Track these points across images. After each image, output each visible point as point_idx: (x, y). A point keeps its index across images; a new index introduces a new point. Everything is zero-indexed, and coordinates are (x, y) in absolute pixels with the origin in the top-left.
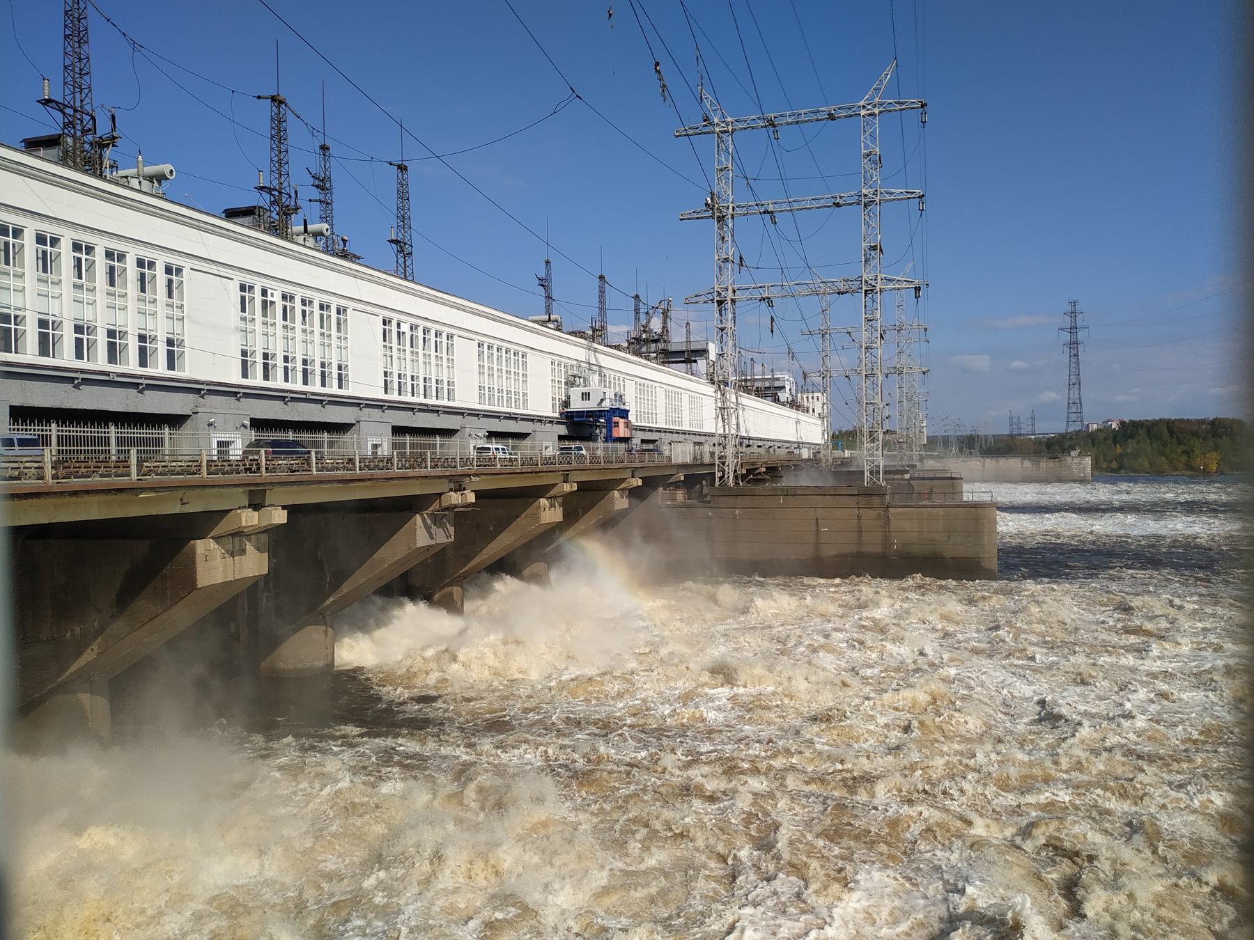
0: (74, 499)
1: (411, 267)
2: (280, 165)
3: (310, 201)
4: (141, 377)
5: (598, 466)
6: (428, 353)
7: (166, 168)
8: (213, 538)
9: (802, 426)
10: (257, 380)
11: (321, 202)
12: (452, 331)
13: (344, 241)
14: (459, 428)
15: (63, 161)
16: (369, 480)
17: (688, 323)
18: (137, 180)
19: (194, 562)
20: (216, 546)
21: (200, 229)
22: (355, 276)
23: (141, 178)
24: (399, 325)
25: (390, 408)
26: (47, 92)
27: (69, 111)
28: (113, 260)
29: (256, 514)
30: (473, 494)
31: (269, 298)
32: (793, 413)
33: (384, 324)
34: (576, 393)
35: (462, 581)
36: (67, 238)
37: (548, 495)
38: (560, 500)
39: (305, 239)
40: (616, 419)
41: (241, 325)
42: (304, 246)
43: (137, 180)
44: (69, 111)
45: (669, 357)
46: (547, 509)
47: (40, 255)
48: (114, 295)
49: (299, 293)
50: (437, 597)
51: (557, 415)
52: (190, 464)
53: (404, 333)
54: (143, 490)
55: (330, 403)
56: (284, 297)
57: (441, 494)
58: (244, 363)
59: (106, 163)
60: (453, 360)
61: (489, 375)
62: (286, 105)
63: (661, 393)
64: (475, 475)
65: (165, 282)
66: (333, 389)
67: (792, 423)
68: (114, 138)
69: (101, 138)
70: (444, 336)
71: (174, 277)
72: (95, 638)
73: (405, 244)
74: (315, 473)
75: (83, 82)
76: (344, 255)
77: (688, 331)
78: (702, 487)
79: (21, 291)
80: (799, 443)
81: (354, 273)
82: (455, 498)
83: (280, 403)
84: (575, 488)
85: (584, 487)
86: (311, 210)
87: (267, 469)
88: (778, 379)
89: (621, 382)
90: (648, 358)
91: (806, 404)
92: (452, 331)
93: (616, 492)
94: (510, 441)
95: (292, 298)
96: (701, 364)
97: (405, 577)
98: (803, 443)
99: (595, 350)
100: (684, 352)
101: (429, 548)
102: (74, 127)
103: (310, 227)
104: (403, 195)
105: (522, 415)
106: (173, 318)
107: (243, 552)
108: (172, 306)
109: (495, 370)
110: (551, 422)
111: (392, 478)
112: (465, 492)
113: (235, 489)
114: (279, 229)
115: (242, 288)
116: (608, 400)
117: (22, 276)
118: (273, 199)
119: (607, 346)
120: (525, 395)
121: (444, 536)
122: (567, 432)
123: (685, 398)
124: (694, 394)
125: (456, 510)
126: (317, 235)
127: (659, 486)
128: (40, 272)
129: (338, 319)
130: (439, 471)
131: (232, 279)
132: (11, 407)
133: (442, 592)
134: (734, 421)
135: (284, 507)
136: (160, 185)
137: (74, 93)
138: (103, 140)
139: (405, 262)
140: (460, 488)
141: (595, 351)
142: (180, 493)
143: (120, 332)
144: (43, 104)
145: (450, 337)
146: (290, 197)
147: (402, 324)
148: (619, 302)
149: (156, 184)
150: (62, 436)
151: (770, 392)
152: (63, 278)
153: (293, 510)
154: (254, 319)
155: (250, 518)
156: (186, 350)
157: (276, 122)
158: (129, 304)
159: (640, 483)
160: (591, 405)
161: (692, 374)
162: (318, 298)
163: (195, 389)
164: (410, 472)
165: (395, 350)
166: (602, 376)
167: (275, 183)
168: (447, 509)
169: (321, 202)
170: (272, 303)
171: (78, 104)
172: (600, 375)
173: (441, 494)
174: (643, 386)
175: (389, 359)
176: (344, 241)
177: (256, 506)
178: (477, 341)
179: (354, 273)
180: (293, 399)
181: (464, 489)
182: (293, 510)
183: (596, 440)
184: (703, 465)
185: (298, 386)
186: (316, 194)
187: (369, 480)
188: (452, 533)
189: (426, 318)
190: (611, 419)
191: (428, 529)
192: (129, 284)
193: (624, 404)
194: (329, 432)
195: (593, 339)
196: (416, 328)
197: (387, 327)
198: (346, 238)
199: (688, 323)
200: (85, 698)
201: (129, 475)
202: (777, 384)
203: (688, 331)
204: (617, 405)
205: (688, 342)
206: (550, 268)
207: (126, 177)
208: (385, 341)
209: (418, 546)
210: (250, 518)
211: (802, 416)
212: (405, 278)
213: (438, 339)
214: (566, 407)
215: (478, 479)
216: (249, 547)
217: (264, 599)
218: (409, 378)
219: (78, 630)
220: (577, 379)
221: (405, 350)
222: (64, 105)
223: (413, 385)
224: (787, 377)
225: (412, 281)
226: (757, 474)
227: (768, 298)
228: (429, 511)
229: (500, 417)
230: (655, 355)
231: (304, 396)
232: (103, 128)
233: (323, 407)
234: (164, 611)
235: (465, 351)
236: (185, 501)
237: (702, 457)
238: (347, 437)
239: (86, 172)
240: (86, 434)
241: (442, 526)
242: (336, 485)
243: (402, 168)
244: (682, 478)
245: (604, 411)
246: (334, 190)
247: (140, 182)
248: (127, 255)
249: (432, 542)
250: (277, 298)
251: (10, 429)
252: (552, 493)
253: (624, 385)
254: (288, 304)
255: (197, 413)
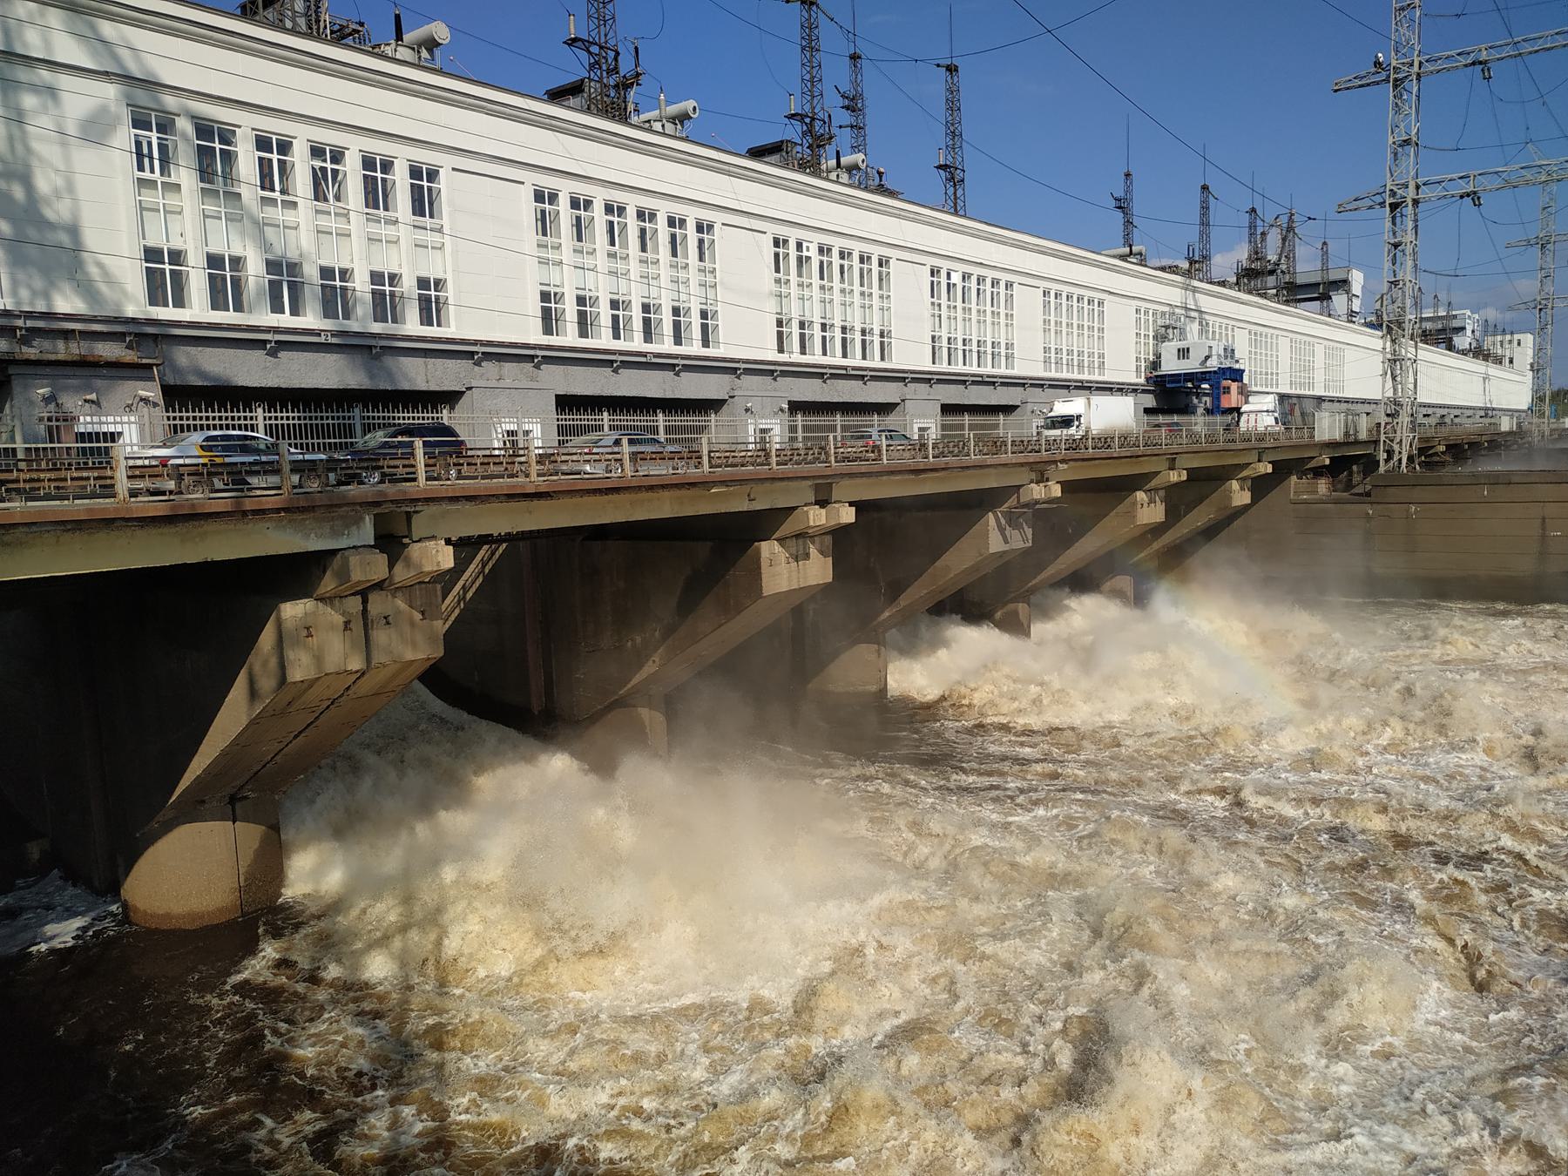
0: (650, 494)
1: (962, 198)
2: (812, 83)
3: (840, 127)
4: (676, 357)
5: (1215, 447)
6: (982, 308)
7: (689, 105)
8: (777, 540)
9: (1493, 385)
10: (569, 337)
11: (852, 127)
12: (887, 252)
13: (880, 174)
14: (1019, 404)
15: (785, 166)
16: (943, 469)
17: (1325, 243)
18: (660, 124)
19: (759, 567)
20: (781, 549)
21: (729, 174)
22: (898, 217)
23: (664, 121)
24: (949, 275)
25: (939, 381)
26: (573, 31)
27: (595, 49)
28: (644, 221)
29: (823, 511)
30: (1059, 485)
31: (805, 253)
32: (1478, 366)
33: (932, 275)
34: (1169, 350)
35: (1025, 597)
36: (355, 148)
37: (1147, 487)
38: (1162, 493)
39: (838, 176)
40: (1225, 383)
41: (774, 288)
42: (837, 182)
43: (660, 124)
44: (595, 49)
45: (1294, 293)
46: (1145, 505)
47: (539, 217)
48: (547, 246)
49: (633, 202)
50: (998, 615)
51: (1142, 380)
52: (728, 454)
53: (954, 285)
54: (715, 483)
55: (874, 378)
56: (821, 251)
57: (1020, 487)
58: (780, 335)
59: (631, 107)
60: (1012, 315)
61: (1056, 333)
62: (818, 6)
63: (1284, 344)
64: (1063, 461)
65: (668, 239)
66: (694, 348)
67: (1477, 382)
68: (638, 75)
69: (624, 77)
70: (1002, 284)
71: (677, 230)
72: (656, 650)
73: (956, 169)
74: (885, 462)
75: (607, 12)
76: (882, 190)
77: (1325, 254)
78: (1351, 474)
79: (396, 242)
80: (1487, 409)
81: (898, 212)
82: (1037, 492)
83: (466, 364)
84: (1184, 478)
85: (1195, 475)
86: (844, 138)
87: (836, 457)
88: (1455, 317)
89: (1274, 341)
90: (1264, 296)
91: (1499, 352)
92: (887, 252)
93: (1234, 482)
94: (967, 417)
95: (653, 216)
96: (1339, 300)
97: (960, 593)
98: (1494, 409)
99: (1195, 290)
100: (1319, 284)
101: (1002, 554)
102: (600, 68)
103: (843, 160)
104: (953, 106)
105: (1097, 382)
106: (705, 286)
107: (807, 556)
108: (646, 262)
109: (1064, 325)
110: (1135, 391)
111: (967, 467)
112: (1050, 483)
113: (804, 482)
114: (810, 165)
115: (776, 243)
116: (1215, 358)
117: (346, 215)
118: (592, 61)
119: (1211, 283)
120: (1101, 356)
121: (1021, 539)
122: (1155, 404)
123: (1319, 350)
124: (1331, 343)
125: (1038, 506)
126: (852, 169)
127: (1291, 474)
128: (540, 237)
129: (880, 273)
130: (1021, 458)
131: (523, 183)
132: (557, 396)
133: (1005, 610)
134: (1411, 379)
135: (851, 504)
136: (682, 126)
137: (598, 27)
138: (627, 80)
139: (955, 193)
140: (1042, 479)
141: (1194, 292)
142: (746, 488)
143: (623, 302)
144: (569, 45)
145: (1009, 285)
146: (825, 123)
147: (952, 273)
148: (1228, 215)
149: (679, 127)
150: (288, 425)
151: (1442, 336)
152: (597, 246)
153: (860, 506)
154: (852, 290)
155: (817, 517)
156: (893, 340)
157: (807, 30)
158: (662, 272)
159: (1270, 469)
160: (1191, 365)
161: (1330, 316)
162: (664, 209)
163: (730, 368)
164: (989, 460)
165: (944, 307)
166: (1204, 326)
167: (807, 108)
168: (1026, 505)
169: (852, 127)
170: (808, 258)
171: (603, 40)
172: (1200, 323)
173: (1020, 487)
174: (1259, 335)
175: (937, 319)
176: (880, 174)
177: (822, 503)
178: (1042, 289)
179: (898, 212)
180: (833, 376)
181: (1047, 480)
182: (860, 506)
183: (1194, 413)
184: (1357, 443)
185: (636, 343)
186: (845, 117)
187: (943, 469)
188: (1030, 537)
189: (981, 264)
190: (1219, 383)
191: (1002, 530)
192: (661, 249)
193: (1237, 361)
194: (366, 406)
195: (1188, 274)
196: (969, 277)
197: (935, 279)
198: (882, 170)
199: (1325, 243)
200: (644, 712)
201: (414, 480)
202: (1456, 324)
203: (1325, 254)
204: (1227, 364)
205: (1325, 269)
206: (1131, 183)
207: (649, 121)
208: (933, 297)
209: (991, 551)
210: (817, 517)
211: (1493, 370)
212: (956, 213)
213: (995, 290)
214: (1156, 370)
215: (1066, 466)
216: (813, 551)
217: (811, 612)
218: (817, 327)
219: (638, 639)
220: (1170, 331)
221: (955, 307)
222: (588, 42)
223: (824, 338)
224: (1469, 313)
225: (964, 216)
226: (1431, 455)
227: (1475, 193)
228: (1004, 508)
229: (965, 381)
230: (1274, 291)
231: (980, 379)
232: (626, 66)
233: (865, 384)
234: (728, 621)
235: (1028, 301)
236: (752, 497)
237: (1356, 431)
238: (1012, 417)
239: (613, 118)
240: (279, 422)
241: (1017, 527)
242: (907, 477)
243: (952, 69)
244: (1327, 462)
245: (1210, 372)
246: (866, 111)
247: (663, 126)
248: (346, 152)
249: (1006, 548)
250: (813, 253)
251: (168, 418)
252: (1153, 484)
253: (1233, 336)
254: (616, 219)
255: (733, 397)
